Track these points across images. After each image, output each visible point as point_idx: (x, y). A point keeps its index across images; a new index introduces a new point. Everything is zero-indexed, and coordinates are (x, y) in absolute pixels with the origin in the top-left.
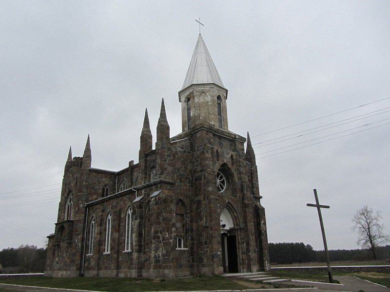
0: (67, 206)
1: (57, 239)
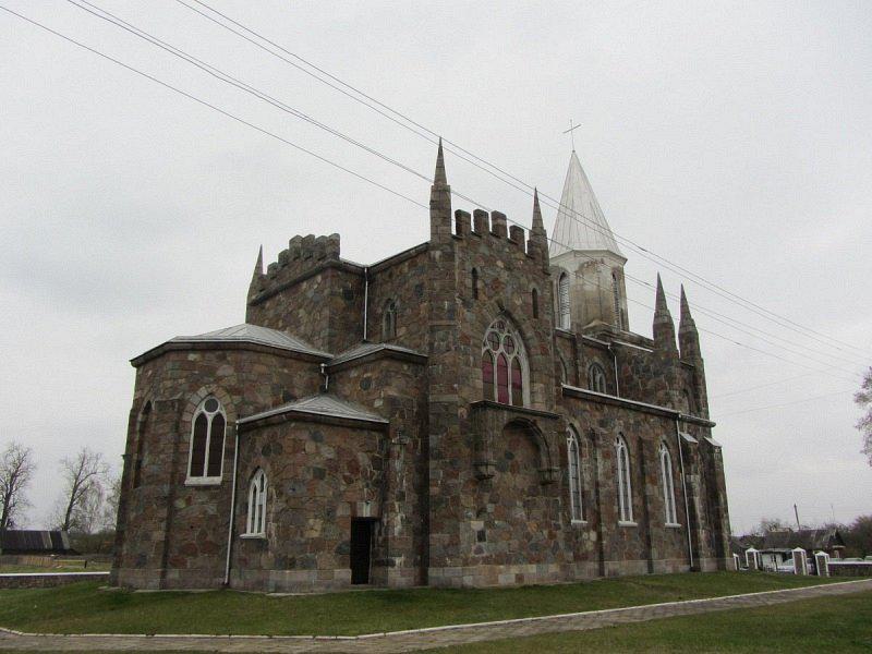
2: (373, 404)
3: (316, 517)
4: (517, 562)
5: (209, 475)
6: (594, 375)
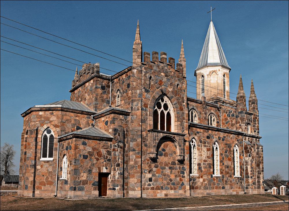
2: (108, 130)
3: (84, 172)
5: (49, 157)
6: (211, 118)
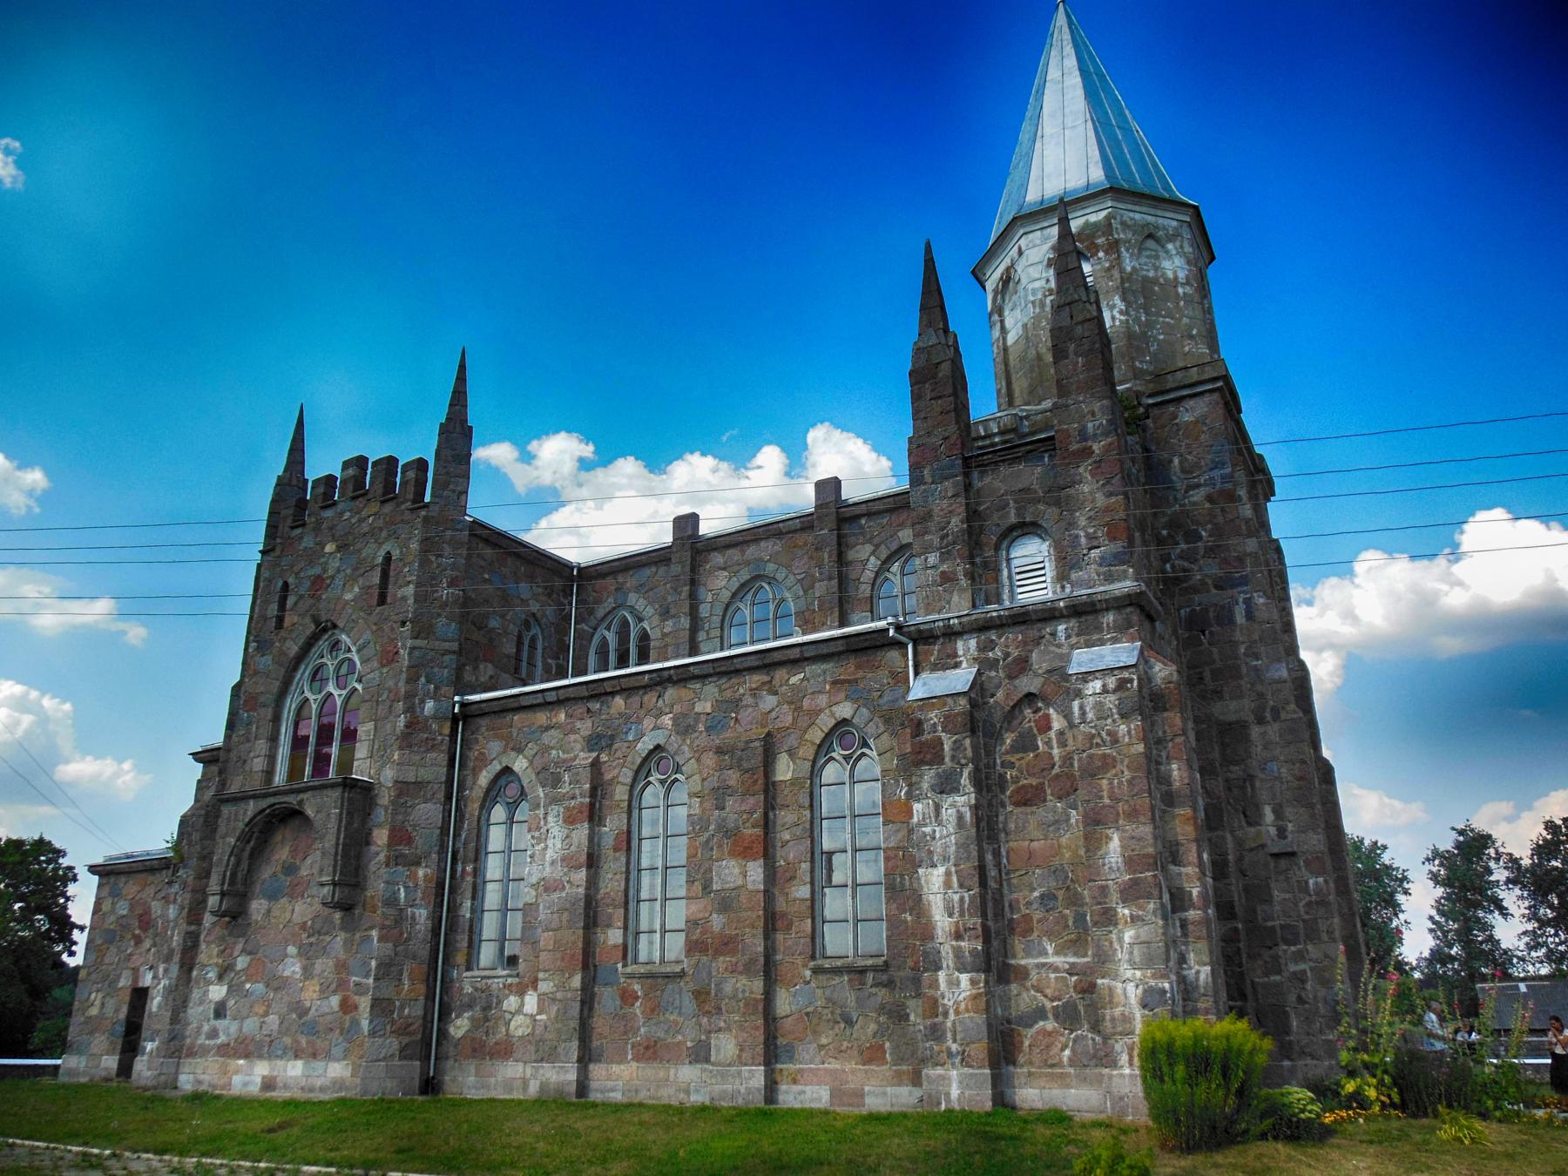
0: (290, 705)
1: (232, 882)
4: (270, 1056)
